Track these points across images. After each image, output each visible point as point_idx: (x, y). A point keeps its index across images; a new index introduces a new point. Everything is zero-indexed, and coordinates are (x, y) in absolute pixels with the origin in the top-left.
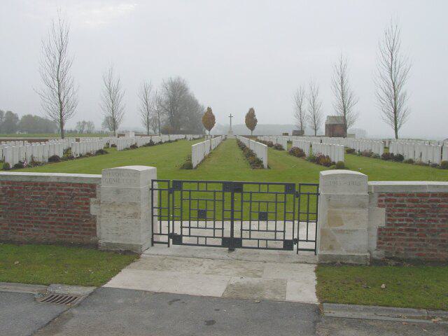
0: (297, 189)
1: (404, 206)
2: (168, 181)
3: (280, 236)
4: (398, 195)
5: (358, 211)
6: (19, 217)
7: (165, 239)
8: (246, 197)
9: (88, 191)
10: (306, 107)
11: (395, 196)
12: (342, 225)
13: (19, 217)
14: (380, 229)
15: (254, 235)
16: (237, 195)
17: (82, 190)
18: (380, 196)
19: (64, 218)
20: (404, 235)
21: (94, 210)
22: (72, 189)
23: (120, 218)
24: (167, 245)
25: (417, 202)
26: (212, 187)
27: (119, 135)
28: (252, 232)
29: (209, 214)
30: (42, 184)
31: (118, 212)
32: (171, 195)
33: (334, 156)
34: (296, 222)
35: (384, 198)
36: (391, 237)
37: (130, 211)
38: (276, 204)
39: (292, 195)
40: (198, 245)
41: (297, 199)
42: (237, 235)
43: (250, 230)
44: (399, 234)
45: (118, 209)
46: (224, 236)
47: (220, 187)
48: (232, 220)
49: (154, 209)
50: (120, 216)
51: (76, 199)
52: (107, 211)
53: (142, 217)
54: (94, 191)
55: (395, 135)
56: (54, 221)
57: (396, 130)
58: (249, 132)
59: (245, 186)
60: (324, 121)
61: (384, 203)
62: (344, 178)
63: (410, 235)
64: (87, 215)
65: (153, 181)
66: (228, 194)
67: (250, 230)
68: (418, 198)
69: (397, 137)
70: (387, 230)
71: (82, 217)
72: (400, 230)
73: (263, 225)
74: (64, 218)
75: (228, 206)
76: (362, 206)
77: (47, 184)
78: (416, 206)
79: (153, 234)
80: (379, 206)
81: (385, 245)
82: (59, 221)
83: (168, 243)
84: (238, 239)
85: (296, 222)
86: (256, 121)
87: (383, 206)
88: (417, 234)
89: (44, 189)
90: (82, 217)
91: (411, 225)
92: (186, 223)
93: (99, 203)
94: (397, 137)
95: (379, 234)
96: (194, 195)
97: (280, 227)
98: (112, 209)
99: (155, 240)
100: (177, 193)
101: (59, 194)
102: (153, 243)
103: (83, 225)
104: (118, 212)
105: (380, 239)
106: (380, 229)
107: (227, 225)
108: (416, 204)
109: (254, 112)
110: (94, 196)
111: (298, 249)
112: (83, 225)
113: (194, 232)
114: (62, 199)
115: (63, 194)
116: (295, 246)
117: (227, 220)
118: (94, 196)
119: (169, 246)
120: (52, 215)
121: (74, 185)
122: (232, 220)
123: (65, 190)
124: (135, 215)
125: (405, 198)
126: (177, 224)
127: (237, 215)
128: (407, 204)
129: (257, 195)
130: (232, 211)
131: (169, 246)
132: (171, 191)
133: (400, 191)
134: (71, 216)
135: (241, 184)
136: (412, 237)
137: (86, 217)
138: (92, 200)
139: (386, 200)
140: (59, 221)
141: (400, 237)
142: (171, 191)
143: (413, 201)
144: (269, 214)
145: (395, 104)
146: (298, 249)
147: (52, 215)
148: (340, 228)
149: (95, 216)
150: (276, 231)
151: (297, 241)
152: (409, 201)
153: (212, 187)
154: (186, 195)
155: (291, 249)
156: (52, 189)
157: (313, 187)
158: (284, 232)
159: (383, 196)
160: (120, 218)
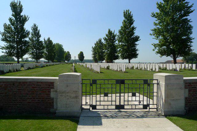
2: (90, 80)
3: (126, 103)
4: (193, 83)
6: (10, 100)
9: (50, 85)
13: (10, 100)
15: (102, 103)
18: (186, 84)
21: (52, 95)
22: (41, 85)
23: (68, 99)
26: (138, 82)
27: (39, 63)
30: (23, 83)
31: (67, 96)
33: (147, 67)
35: (187, 85)
38: (140, 89)
42: (122, 103)
44: (193, 100)
46: (97, 106)
47: (114, 82)
50: (68, 98)
52: (61, 96)
56: (30, 101)
60: (44, 60)
64: (49, 97)
65: (157, 80)
67: (112, 101)
70: (189, 98)
72: (194, 98)
77: (27, 83)
82: (33, 101)
84: (95, 105)
85: (91, 96)
86: (84, 57)
87: (187, 88)
89: (24, 85)
90: (46, 99)
93: (56, 91)
97: (114, 99)
100: (94, 86)
101: (33, 87)
104: (67, 96)
110: (53, 88)
113: (102, 103)
115: (36, 87)
116: (148, 108)
118: (53, 88)
120: (29, 98)
129: (103, 85)
132: (91, 85)
134: (40, 98)
139: (188, 86)
141: (194, 101)
142: (91, 85)
146: (150, 109)
147: (29, 98)
149: (53, 99)
153: (138, 82)
156: (29, 85)
158: (116, 101)
160: (68, 99)
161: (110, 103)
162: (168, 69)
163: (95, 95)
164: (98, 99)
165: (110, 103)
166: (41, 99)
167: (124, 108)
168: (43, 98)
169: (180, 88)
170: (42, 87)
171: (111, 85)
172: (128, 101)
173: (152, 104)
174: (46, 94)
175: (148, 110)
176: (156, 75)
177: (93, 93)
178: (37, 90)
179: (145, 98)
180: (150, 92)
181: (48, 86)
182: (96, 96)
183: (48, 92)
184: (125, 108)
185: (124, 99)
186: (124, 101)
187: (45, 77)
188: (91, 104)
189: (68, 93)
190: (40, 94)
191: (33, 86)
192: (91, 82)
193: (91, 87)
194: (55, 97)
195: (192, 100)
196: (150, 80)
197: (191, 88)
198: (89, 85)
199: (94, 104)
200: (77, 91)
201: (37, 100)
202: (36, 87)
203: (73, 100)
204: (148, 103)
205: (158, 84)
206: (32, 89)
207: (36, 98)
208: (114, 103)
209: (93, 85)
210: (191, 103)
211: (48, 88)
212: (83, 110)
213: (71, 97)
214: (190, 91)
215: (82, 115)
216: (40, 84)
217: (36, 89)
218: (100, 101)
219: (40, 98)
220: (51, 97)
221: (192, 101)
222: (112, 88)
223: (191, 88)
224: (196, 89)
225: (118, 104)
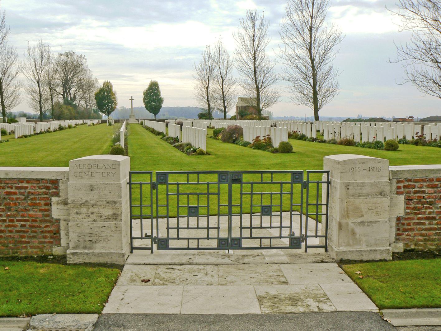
0: (305, 179)
1: (423, 192)
2: (151, 173)
5: (380, 200)
7: (147, 243)
8: (247, 188)
9: (48, 188)
10: (214, 86)
11: (414, 182)
12: (362, 216)
14: (398, 219)
16: (236, 187)
17: (39, 187)
18: (399, 182)
19: (16, 223)
20: (424, 224)
21: (56, 212)
23: (94, 221)
24: (150, 251)
25: (437, 187)
28: (210, 226)
29: (202, 211)
31: (92, 213)
32: (305, 190)
34: (304, 217)
36: (410, 227)
37: (108, 212)
39: (300, 185)
40: (188, 249)
41: (305, 190)
43: (251, 228)
45: (92, 210)
48: (230, 214)
49: (325, 213)
50: (95, 218)
51: (32, 199)
52: (77, 213)
53: (123, 218)
54: (56, 188)
55: (313, 115)
57: (316, 110)
58: (152, 116)
59: (244, 176)
61: (402, 190)
62: (363, 163)
63: (430, 224)
65: (328, 172)
66: (224, 187)
68: (437, 183)
69: (317, 118)
70: (406, 219)
71: (41, 221)
72: (419, 219)
73: (193, 221)
74: (16, 223)
75: (224, 201)
76: (382, 194)
78: (435, 192)
79: (132, 238)
80: (398, 193)
81: (404, 236)
82: (10, 229)
83: (151, 249)
87: (401, 193)
88: (436, 222)
91: (430, 213)
92: (173, 222)
93: (65, 203)
94: (317, 118)
95: (397, 224)
96: (257, 188)
98: (84, 210)
99: (133, 246)
101: (9, 193)
102: (132, 248)
103: (42, 232)
104: (92, 213)
105: (398, 230)
106: (398, 219)
107: (224, 220)
108: (436, 189)
109: (158, 90)
111: (307, 247)
112: (42, 232)
113: (184, 234)
114: (12, 200)
115: (15, 193)
116: (303, 244)
117: (224, 215)
119: (152, 252)
121: (28, 181)
122: (230, 214)
123: (17, 188)
124: (116, 216)
125: (425, 184)
126: (162, 222)
127: (235, 210)
128: (427, 190)
130: (230, 206)
131: (152, 252)
132: (154, 186)
133: (419, 176)
134: (25, 221)
135: (240, 174)
136: (431, 226)
137: (46, 221)
138: (54, 199)
140: (10, 229)
141: (418, 227)
143: (432, 187)
144: (272, 207)
145: (222, 87)
146: (307, 247)
148: (360, 220)
150: (208, 228)
151: (303, 238)
152: (428, 186)
154: (173, 188)
155: (299, 247)
157: (257, 175)
159: (401, 182)
160: (94, 221)
161: (203, 233)
162: (428, 138)
163: (279, 213)
164: (246, 223)
165: (203, 233)
166: (29, 223)
167: (240, 247)
168: (33, 221)
169: (381, 194)
170: (29, 192)
171: (250, 185)
172: (251, 228)
173: (249, 236)
174: (41, 210)
175: (301, 251)
176: (328, 159)
177: (294, 207)
178: (17, 199)
179: (296, 219)
180: (308, 205)
181: (44, 190)
182: (281, 215)
183: (46, 204)
184: (243, 246)
185: (166, 225)
186: (241, 228)
187: (436, 164)
188: (155, 235)
189: (93, 206)
190: (26, 210)
191: (9, 190)
192: (154, 180)
193: (154, 191)
194: (62, 217)
195: (414, 224)
196: (309, 172)
197: (412, 194)
198: (149, 186)
199: (162, 234)
200: (115, 203)
201: (19, 224)
202: (15, 193)
203: (107, 223)
204: (304, 232)
205: (328, 183)
206: (6, 197)
207: (18, 221)
208: (213, 233)
209: (160, 186)
210: (409, 233)
211: (45, 193)
212: (134, 251)
213: (101, 217)
214: (408, 200)
215: (130, 261)
216: (25, 185)
217: (14, 197)
218: (281, 227)
219: (25, 221)
220: (53, 216)
221: (415, 227)
222: (281, 194)
223: (412, 194)
224: (424, 195)
225: (224, 234)
